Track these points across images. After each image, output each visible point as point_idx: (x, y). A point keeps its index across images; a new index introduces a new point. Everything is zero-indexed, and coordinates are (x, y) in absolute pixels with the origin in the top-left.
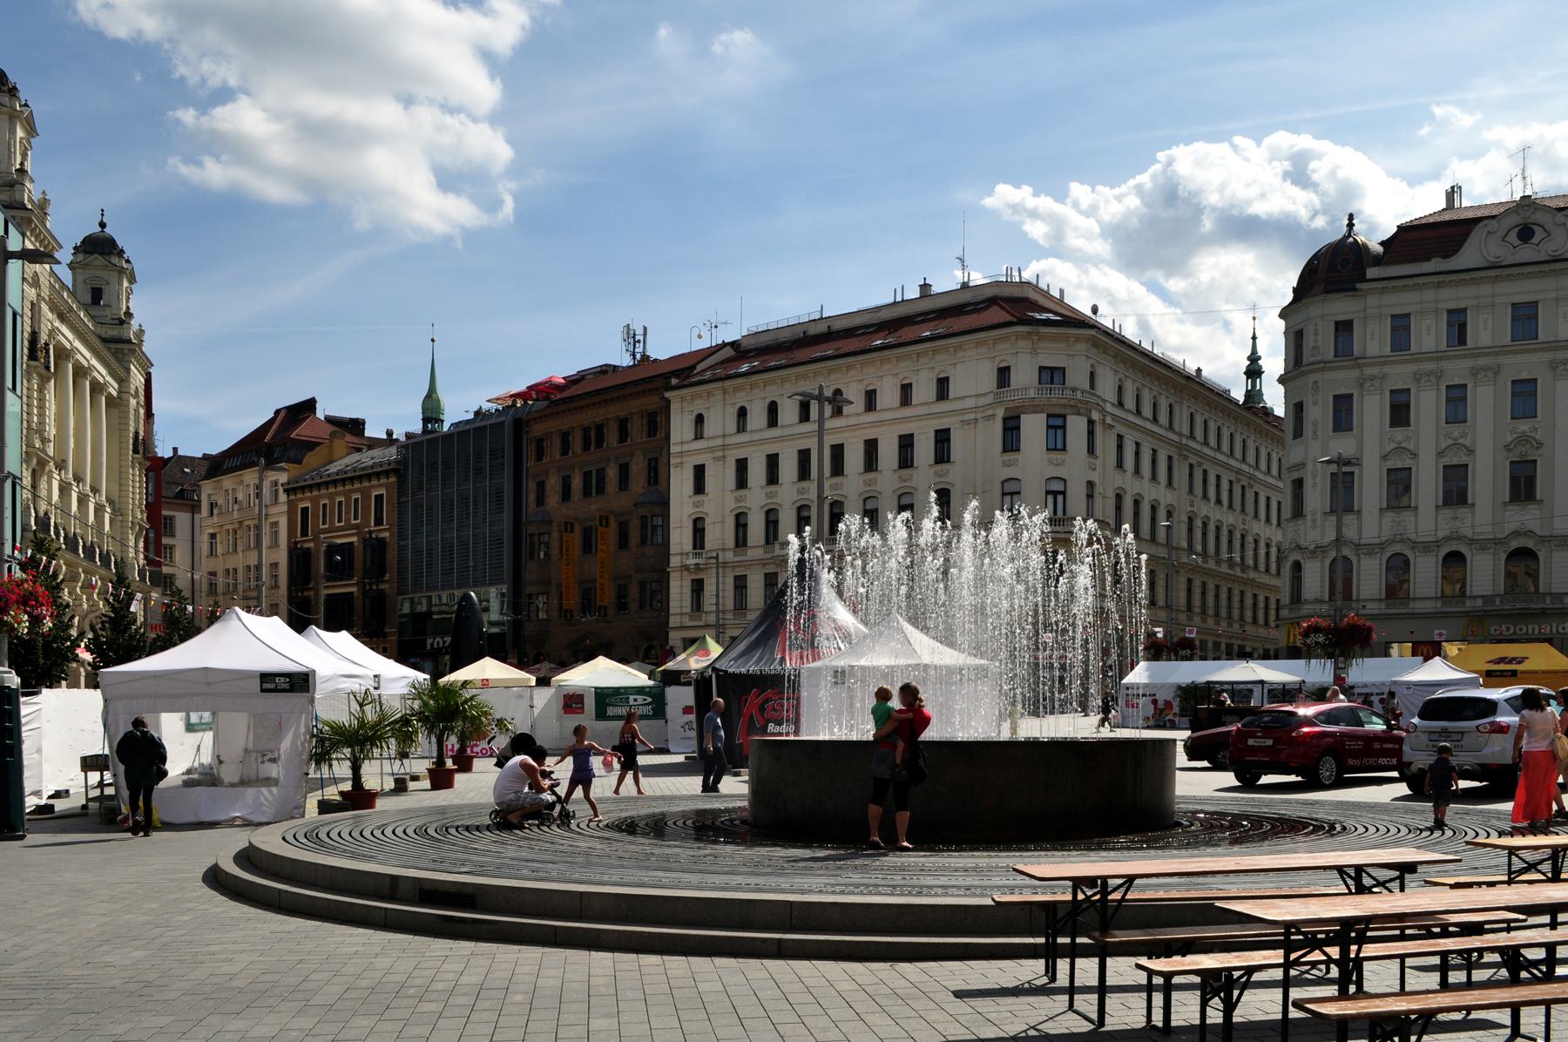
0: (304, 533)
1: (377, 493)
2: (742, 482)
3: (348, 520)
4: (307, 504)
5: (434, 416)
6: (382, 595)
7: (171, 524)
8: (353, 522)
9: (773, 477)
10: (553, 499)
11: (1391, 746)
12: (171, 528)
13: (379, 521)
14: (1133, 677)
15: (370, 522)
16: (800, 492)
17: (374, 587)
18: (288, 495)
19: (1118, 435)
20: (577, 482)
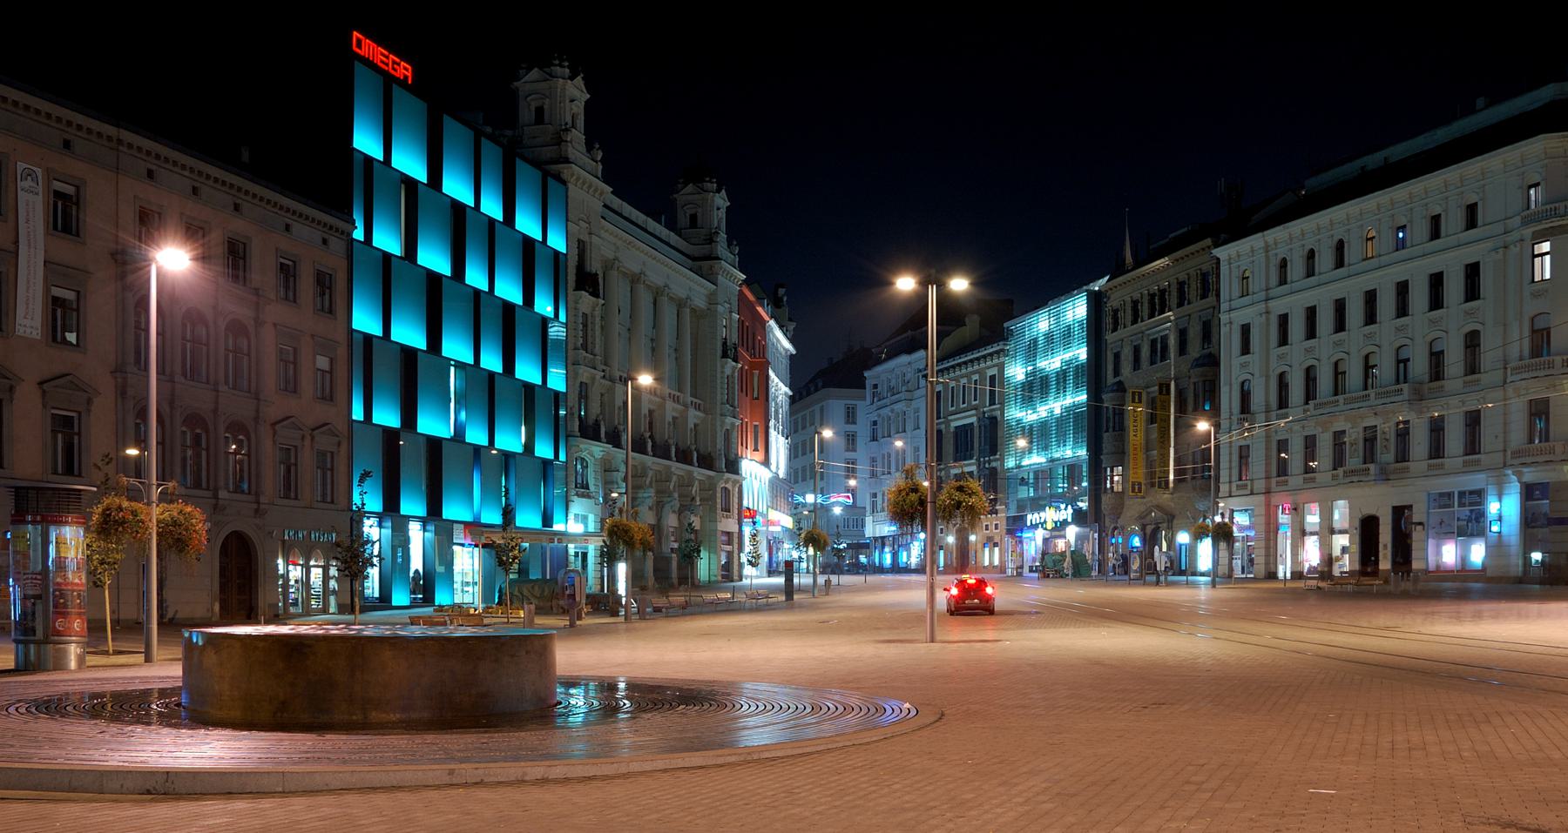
5: (825, 422)
7: (853, 413)
8: (974, 403)
10: (1126, 369)
12: (853, 417)
17: (987, 466)
19: (579, 241)
20: (1145, 352)
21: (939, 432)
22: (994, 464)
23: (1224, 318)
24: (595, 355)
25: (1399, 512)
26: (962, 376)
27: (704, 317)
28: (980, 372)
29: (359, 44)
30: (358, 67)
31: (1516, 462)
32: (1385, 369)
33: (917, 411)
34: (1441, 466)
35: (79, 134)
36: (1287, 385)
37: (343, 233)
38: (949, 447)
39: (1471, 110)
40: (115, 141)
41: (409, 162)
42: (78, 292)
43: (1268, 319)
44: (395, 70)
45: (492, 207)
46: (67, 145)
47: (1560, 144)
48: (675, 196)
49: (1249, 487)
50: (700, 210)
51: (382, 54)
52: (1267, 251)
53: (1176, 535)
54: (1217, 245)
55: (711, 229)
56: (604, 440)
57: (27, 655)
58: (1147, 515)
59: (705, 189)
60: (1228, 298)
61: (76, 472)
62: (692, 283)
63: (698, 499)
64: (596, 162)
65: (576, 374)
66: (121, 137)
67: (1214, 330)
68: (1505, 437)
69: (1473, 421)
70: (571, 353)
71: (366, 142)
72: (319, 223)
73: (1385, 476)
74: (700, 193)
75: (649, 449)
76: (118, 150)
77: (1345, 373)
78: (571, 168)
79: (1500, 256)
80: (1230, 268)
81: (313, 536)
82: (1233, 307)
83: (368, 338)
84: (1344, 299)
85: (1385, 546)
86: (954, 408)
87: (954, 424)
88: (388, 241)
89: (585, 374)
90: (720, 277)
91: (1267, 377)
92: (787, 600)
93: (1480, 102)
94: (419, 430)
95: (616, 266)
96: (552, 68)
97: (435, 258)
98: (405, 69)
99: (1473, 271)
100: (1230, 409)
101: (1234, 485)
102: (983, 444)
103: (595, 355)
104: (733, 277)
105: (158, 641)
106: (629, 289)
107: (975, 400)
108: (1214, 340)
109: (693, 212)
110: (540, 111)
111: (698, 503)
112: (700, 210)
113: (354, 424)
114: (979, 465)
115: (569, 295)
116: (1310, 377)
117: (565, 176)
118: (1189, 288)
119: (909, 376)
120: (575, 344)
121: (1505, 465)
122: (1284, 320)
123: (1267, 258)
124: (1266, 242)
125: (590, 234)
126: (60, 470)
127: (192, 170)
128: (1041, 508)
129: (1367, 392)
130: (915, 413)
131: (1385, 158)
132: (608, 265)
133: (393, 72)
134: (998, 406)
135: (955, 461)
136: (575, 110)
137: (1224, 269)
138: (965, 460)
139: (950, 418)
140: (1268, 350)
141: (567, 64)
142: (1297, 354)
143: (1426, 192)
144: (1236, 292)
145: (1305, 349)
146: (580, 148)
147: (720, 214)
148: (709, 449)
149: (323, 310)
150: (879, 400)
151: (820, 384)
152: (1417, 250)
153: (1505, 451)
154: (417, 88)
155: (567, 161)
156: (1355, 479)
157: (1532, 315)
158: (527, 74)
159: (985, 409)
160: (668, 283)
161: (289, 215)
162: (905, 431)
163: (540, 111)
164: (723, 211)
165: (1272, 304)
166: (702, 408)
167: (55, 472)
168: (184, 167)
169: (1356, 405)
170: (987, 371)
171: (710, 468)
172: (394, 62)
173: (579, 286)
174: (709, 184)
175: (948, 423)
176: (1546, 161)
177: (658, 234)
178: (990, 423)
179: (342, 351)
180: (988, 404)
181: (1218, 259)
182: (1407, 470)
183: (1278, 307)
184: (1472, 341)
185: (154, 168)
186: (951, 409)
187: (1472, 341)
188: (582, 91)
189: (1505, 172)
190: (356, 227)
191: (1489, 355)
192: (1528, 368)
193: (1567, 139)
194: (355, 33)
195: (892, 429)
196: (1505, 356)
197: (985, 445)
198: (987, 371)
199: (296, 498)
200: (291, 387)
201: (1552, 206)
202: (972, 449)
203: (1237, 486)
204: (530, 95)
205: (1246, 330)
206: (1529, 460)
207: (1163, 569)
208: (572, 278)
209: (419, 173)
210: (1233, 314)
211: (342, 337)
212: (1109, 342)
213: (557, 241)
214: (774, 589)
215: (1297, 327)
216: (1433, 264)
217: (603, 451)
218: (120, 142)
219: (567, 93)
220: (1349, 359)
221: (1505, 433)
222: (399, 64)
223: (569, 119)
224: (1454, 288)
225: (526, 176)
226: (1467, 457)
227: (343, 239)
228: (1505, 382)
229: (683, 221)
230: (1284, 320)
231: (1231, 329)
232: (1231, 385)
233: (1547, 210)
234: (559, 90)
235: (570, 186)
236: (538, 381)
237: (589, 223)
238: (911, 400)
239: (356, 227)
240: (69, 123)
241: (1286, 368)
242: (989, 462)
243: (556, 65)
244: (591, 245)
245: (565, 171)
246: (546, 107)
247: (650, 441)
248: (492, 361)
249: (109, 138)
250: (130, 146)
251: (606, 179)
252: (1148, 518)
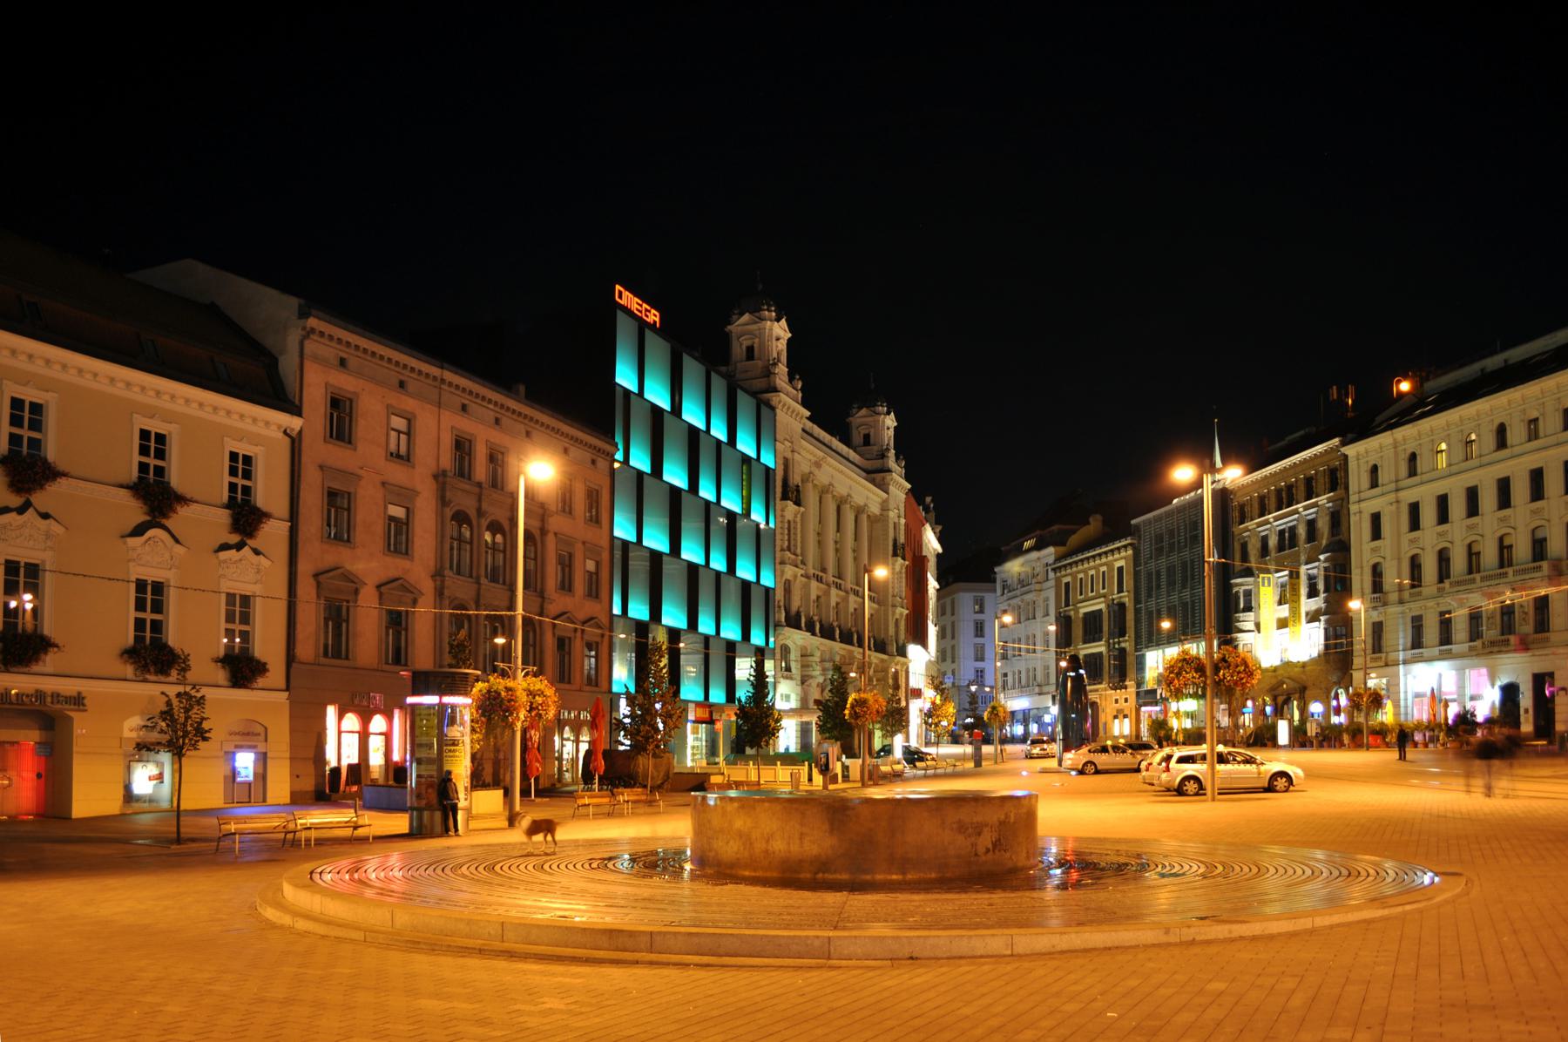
0: (1067, 604)
1: (1066, 581)
2: (1415, 524)
3: (1098, 591)
4: (1068, 579)
6: (1123, 651)
8: (1102, 591)
9: (1443, 517)
11: (1069, 685)
13: (1120, 590)
14: (1243, 668)
15: (1113, 591)
16: (1469, 528)
17: (1117, 646)
18: (1055, 573)
22: (1123, 645)
23: (1353, 508)
25: (1540, 680)
26: (1090, 569)
27: (878, 521)
33: (1046, 599)
35: (412, 375)
38: (1078, 630)
40: (439, 380)
41: (658, 394)
42: (408, 509)
43: (1398, 508)
44: (647, 316)
45: (719, 431)
46: (402, 385)
49: (1383, 659)
50: (872, 431)
51: (638, 304)
53: (1308, 704)
57: (420, 818)
58: (1278, 687)
61: (403, 661)
63: (875, 679)
64: (797, 390)
65: (783, 573)
66: (444, 377)
70: (778, 555)
71: (625, 377)
73: (1525, 646)
75: (837, 636)
76: (440, 388)
78: (779, 396)
81: (582, 716)
83: (625, 544)
85: (1526, 711)
86: (1094, 594)
87: (1082, 611)
88: (640, 460)
89: (789, 571)
90: (891, 487)
91: (1399, 559)
92: (976, 766)
94: (663, 623)
98: (655, 315)
101: (1368, 658)
102: (1112, 627)
104: (899, 486)
106: (818, 499)
107: (1104, 588)
108: (1344, 528)
110: (750, 349)
114: (1109, 646)
116: (1443, 558)
117: (773, 403)
119: (1038, 570)
122: (1414, 509)
123: (1396, 453)
124: (1395, 440)
125: (793, 451)
126: (390, 661)
127: (496, 404)
128: (486, 728)
129: (1472, 576)
130: (1044, 601)
132: (806, 478)
133: (644, 317)
134: (1126, 594)
135: (1085, 643)
136: (780, 347)
137: (1352, 465)
138: (1094, 642)
139: (1079, 605)
140: (1399, 535)
142: (1430, 537)
143: (1558, 387)
146: (784, 379)
150: (1010, 591)
152: (1552, 440)
154: (663, 331)
156: (1496, 649)
160: (851, 492)
163: (750, 349)
164: (892, 430)
165: (1402, 494)
167: (387, 663)
168: (490, 401)
169: (1493, 582)
170: (1115, 563)
172: (646, 310)
173: (785, 497)
174: (880, 408)
175: (1077, 610)
179: (605, 556)
180: (1116, 592)
183: (1409, 496)
185: (466, 402)
186: (1079, 597)
188: (785, 331)
190: (619, 450)
195: (1022, 617)
197: (1114, 628)
198: (1115, 563)
199: (569, 682)
200: (566, 586)
202: (1101, 631)
203: (1371, 658)
204: (741, 336)
205: (1376, 519)
209: (664, 403)
210: (1363, 505)
211: (605, 543)
213: (768, 459)
215: (1428, 514)
217: (804, 639)
218: (443, 381)
219: (774, 333)
220: (1516, 534)
222: (649, 311)
223: (775, 355)
225: (745, 404)
227: (607, 460)
229: (857, 438)
230: (1414, 509)
231: (1360, 518)
232: (1362, 568)
235: (778, 411)
238: (1040, 591)
239: (619, 450)
240: (405, 366)
241: (1418, 551)
242: (1119, 643)
246: (755, 346)
249: (435, 378)
250: (450, 384)
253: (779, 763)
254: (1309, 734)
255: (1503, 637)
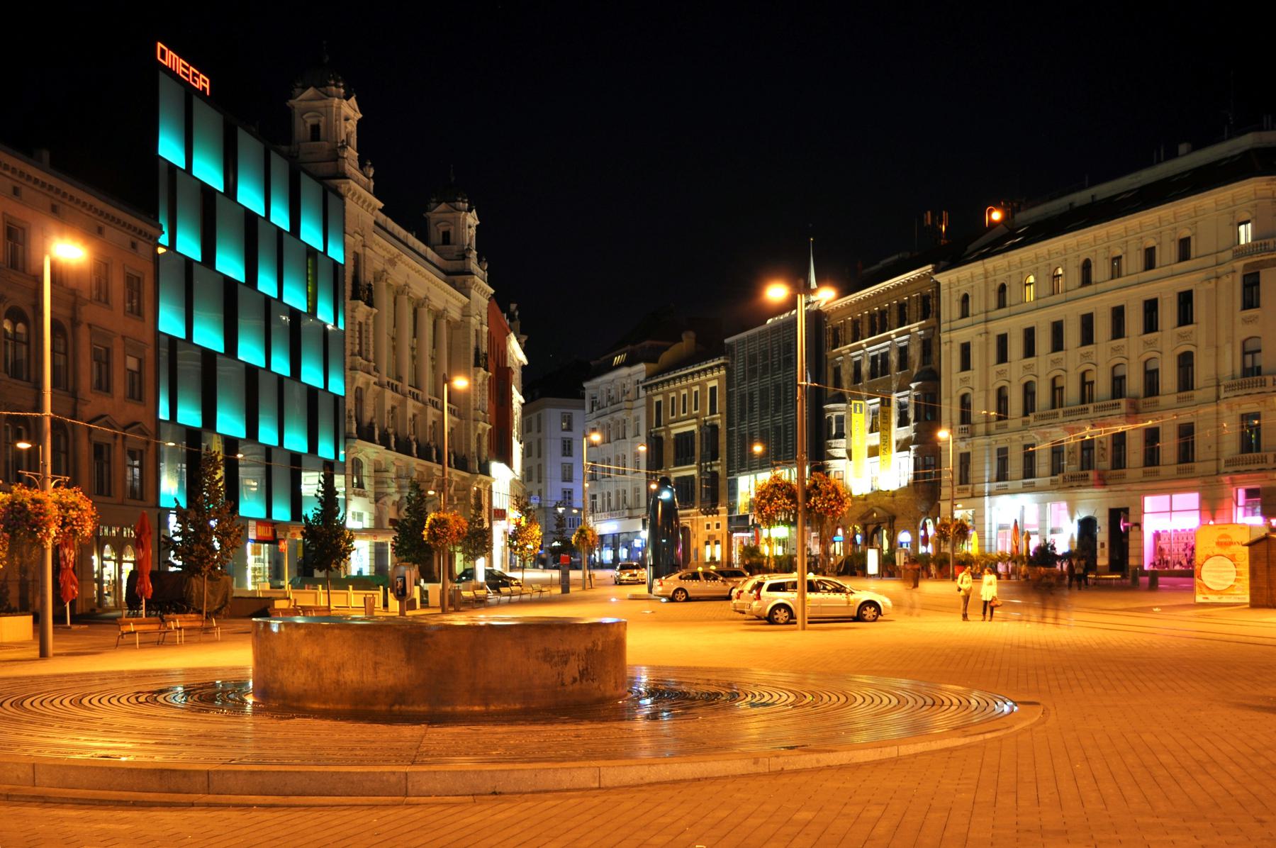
8: (694, 412)
17: (709, 470)
21: (659, 439)
23: (944, 337)
24: (369, 361)
27: (458, 327)
28: (702, 385)
29: (163, 56)
30: (162, 76)
31: (1230, 469)
32: (1103, 386)
33: (637, 419)
34: (1157, 473)
36: (1006, 399)
37: (151, 237)
38: (669, 452)
39: (1173, 154)
41: (208, 172)
43: (987, 339)
45: (280, 218)
47: (1268, 187)
48: (428, 214)
49: (970, 491)
50: (452, 228)
51: (183, 66)
52: (986, 278)
54: (936, 271)
55: (463, 246)
56: (378, 442)
59: (457, 207)
60: (948, 319)
62: (448, 296)
63: (455, 498)
64: (369, 178)
65: (353, 379)
67: (934, 348)
68: (1217, 448)
69: (1186, 432)
70: (348, 360)
71: (170, 149)
72: (124, 224)
73: (1102, 482)
74: (452, 212)
75: (414, 451)
77: (1062, 388)
78: (348, 183)
79: (1212, 285)
80: (950, 292)
81: (125, 533)
82: (953, 327)
83: (173, 340)
84: (1062, 321)
85: (1102, 545)
87: (674, 432)
88: (189, 246)
89: (361, 379)
90: (472, 291)
91: (987, 391)
93: (1183, 148)
95: (384, 278)
96: (328, 88)
97: (230, 265)
99: (1185, 299)
100: (951, 419)
102: (704, 450)
103: (369, 361)
104: (482, 291)
105: (54, 638)
107: (696, 409)
108: (934, 357)
109: (446, 229)
110: (315, 129)
111: (456, 502)
112: (452, 228)
113: (162, 424)
115: (347, 305)
116: (1029, 392)
118: (909, 309)
120: (352, 350)
121: (1218, 473)
122: (1002, 340)
123: (987, 284)
124: (986, 270)
127: (14, 170)
129: (1085, 406)
131: (1093, 196)
132: (379, 276)
134: (719, 415)
135: (676, 465)
137: (944, 293)
139: (671, 426)
140: (987, 366)
141: (341, 84)
142: (1016, 370)
144: (956, 311)
145: (1024, 367)
147: (471, 232)
148: (464, 452)
149: (132, 312)
150: (599, 409)
151: (537, 394)
153: (1218, 459)
155: (344, 176)
156: (1075, 484)
157: (1245, 337)
158: (302, 93)
159: (707, 418)
161: (102, 218)
162: (625, 438)
163: (315, 129)
164: (474, 229)
165: (991, 325)
166: (456, 412)
171: (465, 469)
172: (194, 74)
173: (355, 296)
175: (668, 430)
176: (1256, 201)
177: (416, 249)
178: (711, 431)
179: (149, 352)
180: (708, 413)
181: (938, 284)
182: (1123, 476)
183: (998, 327)
184: (1186, 361)
186: (671, 418)
187: (1186, 361)
189: (1217, 210)
190: (163, 233)
191: (1203, 371)
192: (1242, 386)
193: (1275, 182)
194: (160, 45)
196: (1217, 375)
199: (109, 495)
200: (104, 385)
201: (1263, 242)
202: (693, 454)
203: (958, 489)
205: (966, 348)
206: (1242, 468)
207: (902, 564)
208: (349, 288)
210: (954, 334)
211: (148, 337)
212: (829, 357)
214: (549, 583)
215: (1016, 347)
216: (1148, 292)
219: (342, 111)
221: (1217, 443)
222: (198, 77)
223: (344, 137)
224: (1167, 314)
225: (310, 190)
226: (1181, 465)
227: (149, 244)
228: (1218, 398)
229: (436, 236)
230: (1002, 340)
232: (951, 398)
233: (1261, 244)
234: (334, 109)
235: (348, 200)
236: (320, 385)
237: (363, 236)
238: (631, 409)
239: (163, 233)
242: (711, 466)
243: (332, 85)
244: (365, 258)
245: (343, 186)
247: (414, 443)
248: (281, 365)
251: (377, 193)
252: (870, 518)
253: (351, 587)
254: (898, 564)
255: (1082, 473)
